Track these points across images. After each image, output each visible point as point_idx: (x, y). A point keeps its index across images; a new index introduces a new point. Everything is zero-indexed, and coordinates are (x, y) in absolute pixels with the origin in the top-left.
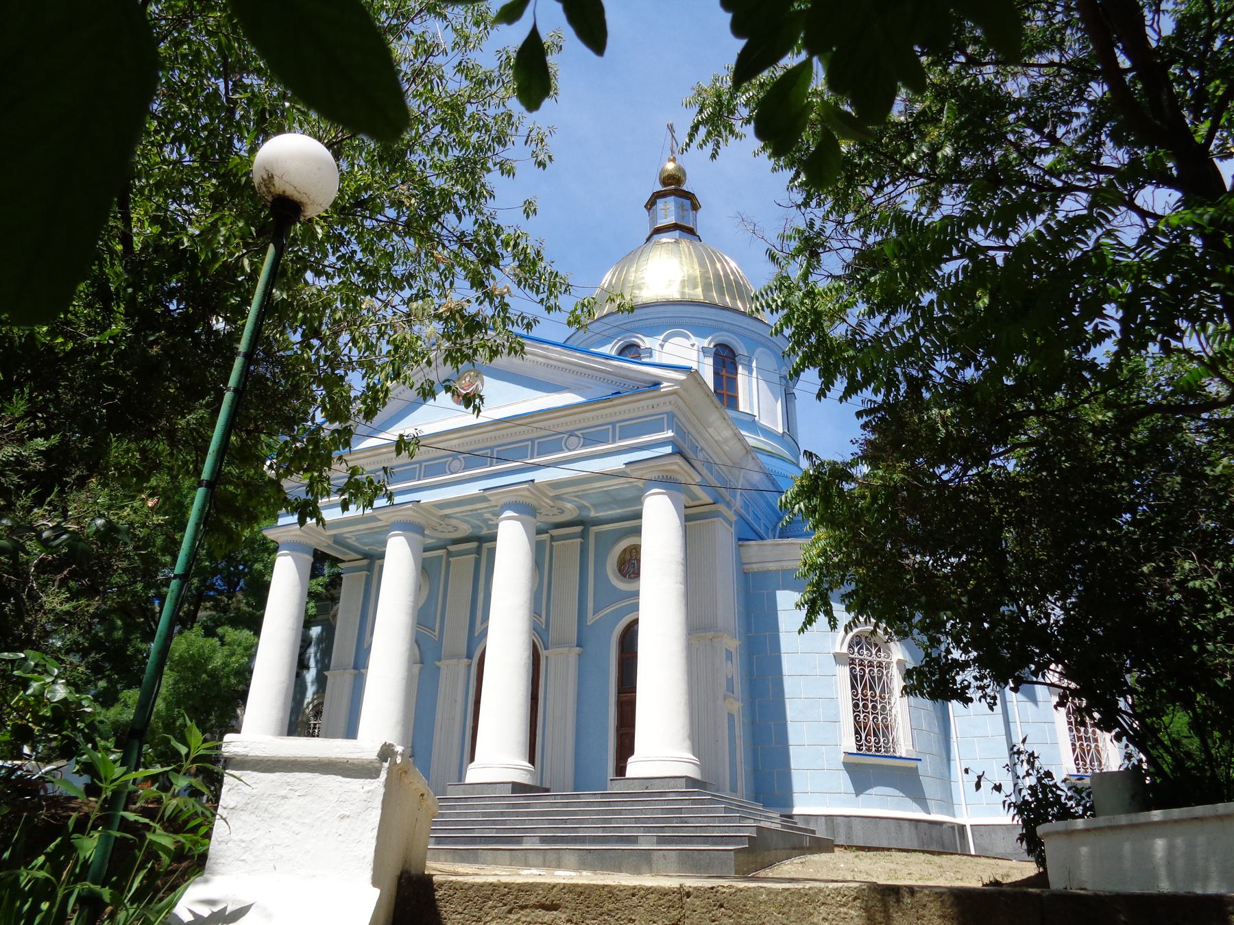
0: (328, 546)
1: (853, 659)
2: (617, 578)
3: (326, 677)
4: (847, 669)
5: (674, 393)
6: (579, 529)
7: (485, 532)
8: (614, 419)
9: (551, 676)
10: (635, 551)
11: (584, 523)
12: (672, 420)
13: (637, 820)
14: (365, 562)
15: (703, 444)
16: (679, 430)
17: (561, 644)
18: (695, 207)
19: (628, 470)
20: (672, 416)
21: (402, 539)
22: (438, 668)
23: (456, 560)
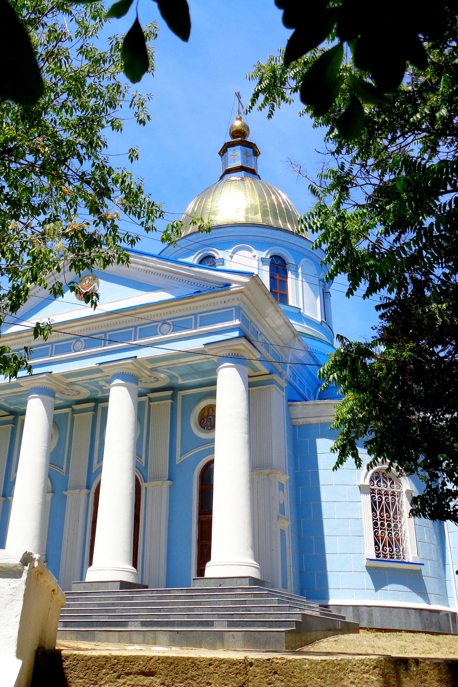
1: (373, 490)
2: (198, 429)
4: (369, 497)
6: (169, 393)
7: (100, 395)
10: (211, 409)
11: (173, 389)
12: (239, 312)
13: (213, 609)
14: (11, 417)
15: (262, 329)
16: (244, 320)
17: (156, 478)
18: (256, 153)
20: (238, 309)
22: (66, 496)
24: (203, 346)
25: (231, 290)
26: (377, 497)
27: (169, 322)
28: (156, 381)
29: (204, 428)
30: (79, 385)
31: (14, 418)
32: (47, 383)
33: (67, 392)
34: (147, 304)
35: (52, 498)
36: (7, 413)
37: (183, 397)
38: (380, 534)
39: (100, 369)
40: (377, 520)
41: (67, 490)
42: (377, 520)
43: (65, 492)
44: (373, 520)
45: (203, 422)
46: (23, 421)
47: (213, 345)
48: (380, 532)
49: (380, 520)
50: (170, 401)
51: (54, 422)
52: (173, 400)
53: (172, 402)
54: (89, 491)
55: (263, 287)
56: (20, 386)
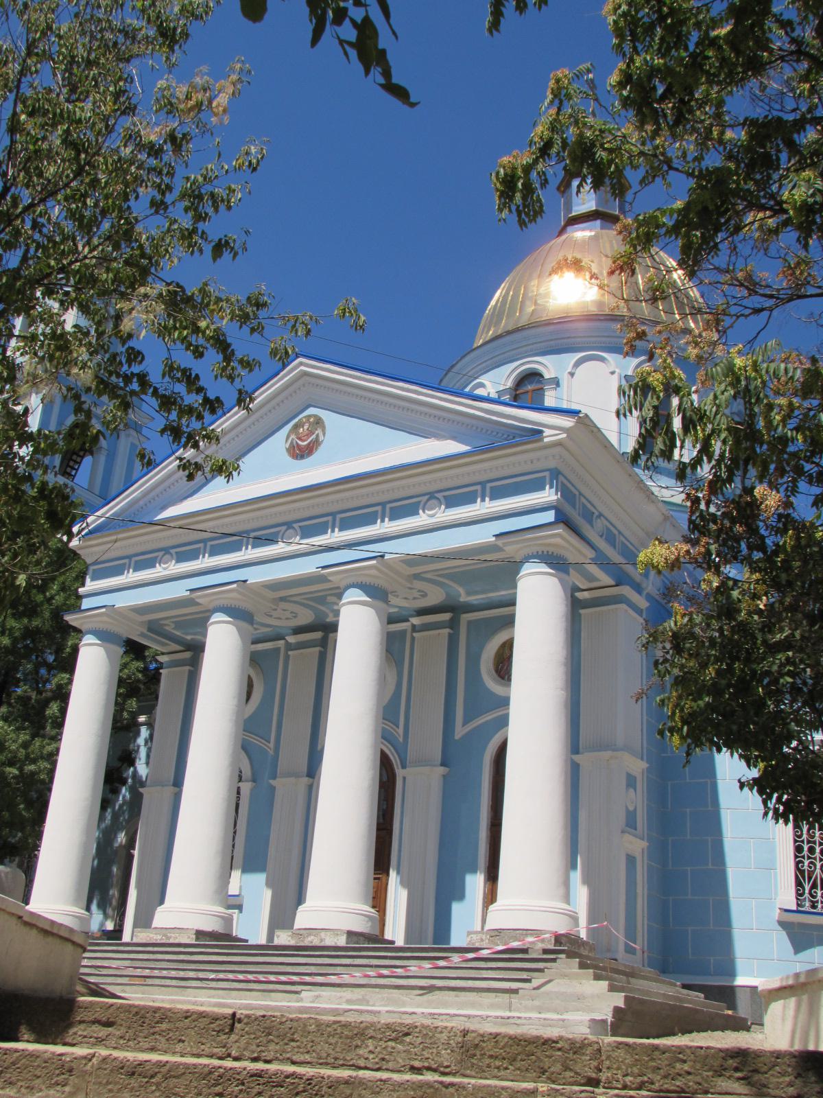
0: (142, 635)
3: (141, 795)
5: (559, 444)
6: (446, 616)
8: (485, 477)
10: (508, 646)
11: (454, 609)
14: (188, 655)
15: (602, 508)
16: (568, 494)
17: (423, 762)
19: (500, 543)
20: (555, 474)
22: (273, 788)
23: (291, 648)
24: (188, 593)
27: (439, 495)
30: (295, 602)
33: (275, 614)
35: (252, 790)
36: (179, 648)
37: (469, 622)
38: (806, 867)
40: (803, 842)
41: (274, 777)
42: (803, 842)
43: (271, 781)
44: (795, 841)
45: (502, 667)
46: (336, 641)
47: (512, 535)
48: (806, 862)
49: (809, 842)
50: (447, 631)
52: (452, 628)
54: (311, 780)
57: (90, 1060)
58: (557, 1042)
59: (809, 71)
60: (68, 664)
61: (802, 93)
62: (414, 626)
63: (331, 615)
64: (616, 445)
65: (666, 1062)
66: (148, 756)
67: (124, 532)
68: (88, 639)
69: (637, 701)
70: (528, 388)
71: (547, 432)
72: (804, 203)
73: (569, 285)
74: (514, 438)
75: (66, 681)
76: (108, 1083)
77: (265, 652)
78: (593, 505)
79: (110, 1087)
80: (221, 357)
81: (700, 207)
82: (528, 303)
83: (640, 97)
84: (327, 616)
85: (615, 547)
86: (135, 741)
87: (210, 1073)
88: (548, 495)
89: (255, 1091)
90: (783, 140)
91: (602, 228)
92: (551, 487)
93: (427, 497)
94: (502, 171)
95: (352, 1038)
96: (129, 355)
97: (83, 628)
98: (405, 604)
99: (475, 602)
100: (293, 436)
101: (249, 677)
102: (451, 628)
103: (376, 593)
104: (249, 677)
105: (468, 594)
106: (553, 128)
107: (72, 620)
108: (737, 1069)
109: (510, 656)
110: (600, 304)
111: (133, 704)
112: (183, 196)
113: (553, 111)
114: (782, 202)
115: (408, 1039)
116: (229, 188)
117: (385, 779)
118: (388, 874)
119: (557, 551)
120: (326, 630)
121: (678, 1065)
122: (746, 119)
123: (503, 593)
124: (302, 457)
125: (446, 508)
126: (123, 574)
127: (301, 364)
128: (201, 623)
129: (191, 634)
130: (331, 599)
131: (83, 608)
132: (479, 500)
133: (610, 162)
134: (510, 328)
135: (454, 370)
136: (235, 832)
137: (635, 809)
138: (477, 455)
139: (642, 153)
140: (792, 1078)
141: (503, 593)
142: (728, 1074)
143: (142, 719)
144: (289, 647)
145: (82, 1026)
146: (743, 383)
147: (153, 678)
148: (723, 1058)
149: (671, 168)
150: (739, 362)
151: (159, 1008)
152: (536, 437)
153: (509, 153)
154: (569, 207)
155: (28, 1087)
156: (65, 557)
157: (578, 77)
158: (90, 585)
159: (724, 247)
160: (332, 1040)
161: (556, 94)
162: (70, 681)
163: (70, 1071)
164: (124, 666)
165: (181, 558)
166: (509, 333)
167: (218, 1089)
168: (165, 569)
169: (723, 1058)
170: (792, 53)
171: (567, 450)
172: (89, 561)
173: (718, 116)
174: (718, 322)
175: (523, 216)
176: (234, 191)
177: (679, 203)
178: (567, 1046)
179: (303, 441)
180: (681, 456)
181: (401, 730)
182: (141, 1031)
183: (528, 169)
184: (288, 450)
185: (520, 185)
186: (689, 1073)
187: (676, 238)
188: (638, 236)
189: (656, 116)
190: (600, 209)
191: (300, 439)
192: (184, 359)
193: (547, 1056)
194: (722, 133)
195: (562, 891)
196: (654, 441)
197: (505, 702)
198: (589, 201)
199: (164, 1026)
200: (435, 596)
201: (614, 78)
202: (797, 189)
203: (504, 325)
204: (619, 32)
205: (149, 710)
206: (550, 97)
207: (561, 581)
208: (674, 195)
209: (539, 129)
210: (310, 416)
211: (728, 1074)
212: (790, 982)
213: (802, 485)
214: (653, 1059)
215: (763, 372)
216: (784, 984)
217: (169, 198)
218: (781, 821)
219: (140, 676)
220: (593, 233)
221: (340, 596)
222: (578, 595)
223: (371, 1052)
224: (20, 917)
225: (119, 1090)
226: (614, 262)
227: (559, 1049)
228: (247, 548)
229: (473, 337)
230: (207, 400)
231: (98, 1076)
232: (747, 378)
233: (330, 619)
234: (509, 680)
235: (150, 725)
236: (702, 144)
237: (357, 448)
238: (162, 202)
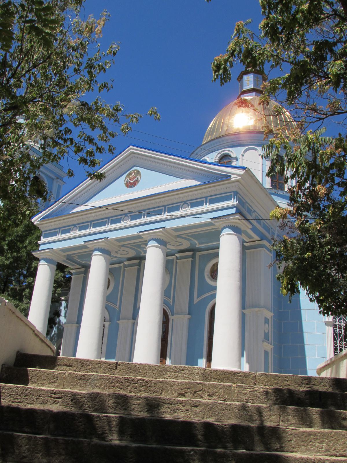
0: (64, 261)
1: (336, 325)
2: (210, 279)
4: (331, 328)
5: (237, 181)
6: (191, 253)
8: (206, 195)
9: (174, 337)
10: (216, 265)
11: (193, 250)
12: (236, 194)
14: (83, 269)
15: (255, 208)
16: (241, 201)
17: (179, 313)
19: (213, 222)
20: (236, 193)
21: (102, 258)
23: (127, 265)
24: (84, 243)
25: (232, 179)
26: (338, 330)
27: (188, 202)
28: (128, 253)
29: (214, 279)
31: (85, 270)
32: (162, 236)
33: (119, 252)
34: (161, 193)
35: (109, 325)
36: (80, 267)
37: (200, 256)
39: (86, 245)
41: (119, 320)
42: (337, 346)
44: (334, 346)
46: (145, 263)
49: (340, 346)
50: (191, 259)
51: (110, 271)
53: (193, 259)
55: (254, 177)
56: (213, 225)
57: (65, 374)
58: (239, 373)
59: (339, 22)
60: (33, 274)
61: (337, 32)
62: (177, 257)
63: (143, 253)
64: (261, 182)
65: (280, 381)
66: (65, 314)
67: (57, 218)
68: (42, 262)
69: (269, 268)
70: (225, 160)
71: (233, 176)
72: (337, 74)
73: (242, 119)
74: (219, 179)
75: (32, 281)
76: (71, 382)
77: (115, 268)
78: (251, 207)
79: (72, 383)
80: (102, 131)
81: (295, 75)
82: (225, 126)
83: (272, 32)
84: (141, 253)
85: (260, 225)
86: (60, 308)
87: (110, 378)
88: (233, 202)
89: (127, 385)
90: (328, 49)
91: (256, 95)
92: (234, 199)
93: (183, 203)
94: (216, 62)
95: (162, 371)
96: (66, 130)
97: (40, 258)
98: (174, 248)
99: (203, 247)
100: (128, 178)
101: (109, 279)
102: (192, 258)
103: (162, 243)
104: (109, 279)
105: (200, 244)
106: (236, 45)
107: (36, 254)
108: (307, 384)
109: (217, 270)
110: (255, 126)
111: (59, 290)
112: (86, 68)
113: (236, 38)
114: (328, 74)
115: (183, 372)
116: (106, 62)
117: (165, 320)
118: (166, 359)
119: (236, 225)
120: (141, 259)
121: (285, 382)
122: (314, 42)
123: (214, 243)
124: (131, 187)
125: (191, 207)
126: (57, 235)
127: (131, 149)
128: (89, 256)
129: (85, 261)
130: (143, 246)
131: (40, 249)
132: (204, 204)
133: (259, 59)
134: (217, 136)
135: (195, 153)
136: (102, 343)
137: (268, 332)
138: (205, 185)
139: (272, 56)
140: (328, 387)
141: (214, 243)
142: (304, 386)
143: (63, 298)
144: (125, 266)
145: (60, 367)
146: (312, 145)
147: (68, 280)
148: (302, 380)
149: (283, 61)
150: (310, 136)
151: (89, 360)
152: (228, 178)
153: (218, 55)
154: (242, 87)
155: (41, 384)
156: (31, 229)
157: (246, 24)
158: (43, 240)
159: (305, 93)
160: (154, 372)
161: (238, 32)
162: (34, 281)
163: (57, 378)
164: (56, 275)
165: (81, 229)
166: (217, 138)
167: (113, 384)
168: (74, 233)
169: (302, 380)
170: (332, 15)
171: (241, 183)
172: (42, 230)
173: (303, 41)
174: (302, 125)
175: (223, 81)
176: (108, 63)
177: (287, 75)
178: (243, 375)
179: (132, 180)
180: (287, 173)
181: (171, 300)
182: (82, 368)
183: (226, 61)
184: (125, 184)
185: (222, 67)
186: (289, 385)
187: (286, 89)
188: (270, 88)
189: (278, 39)
190: (255, 88)
191: (130, 179)
192: (89, 132)
193: (235, 378)
194: (305, 48)
195: (238, 364)
196: (276, 175)
197: (215, 288)
198: (250, 84)
199: (91, 367)
200: (186, 245)
201: (262, 25)
202: (335, 67)
203: (215, 135)
204: (264, 7)
205: (66, 294)
206: (235, 32)
207: (238, 237)
208: (285, 72)
209: (231, 45)
210: (134, 170)
211: (304, 386)
212: (329, 362)
213: (336, 187)
214: (275, 380)
215: (320, 140)
216: (326, 363)
217: (81, 68)
218: (326, 315)
219: (62, 279)
220: (252, 98)
221: (146, 245)
222: (245, 244)
223: (169, 376)
224: (34, 331)
225: (76, 385)
226: (261, 100)
227: (240, 376)
228: (108, 224)
229: (202, 142)
230: (98, 148)
231: (67, 380)
232: (314, 143)
233: (142, 254)
234: (217, 279)
235: (67, 301)
236: (296, 52)
237: (154, 183)
238: (79, 70)
